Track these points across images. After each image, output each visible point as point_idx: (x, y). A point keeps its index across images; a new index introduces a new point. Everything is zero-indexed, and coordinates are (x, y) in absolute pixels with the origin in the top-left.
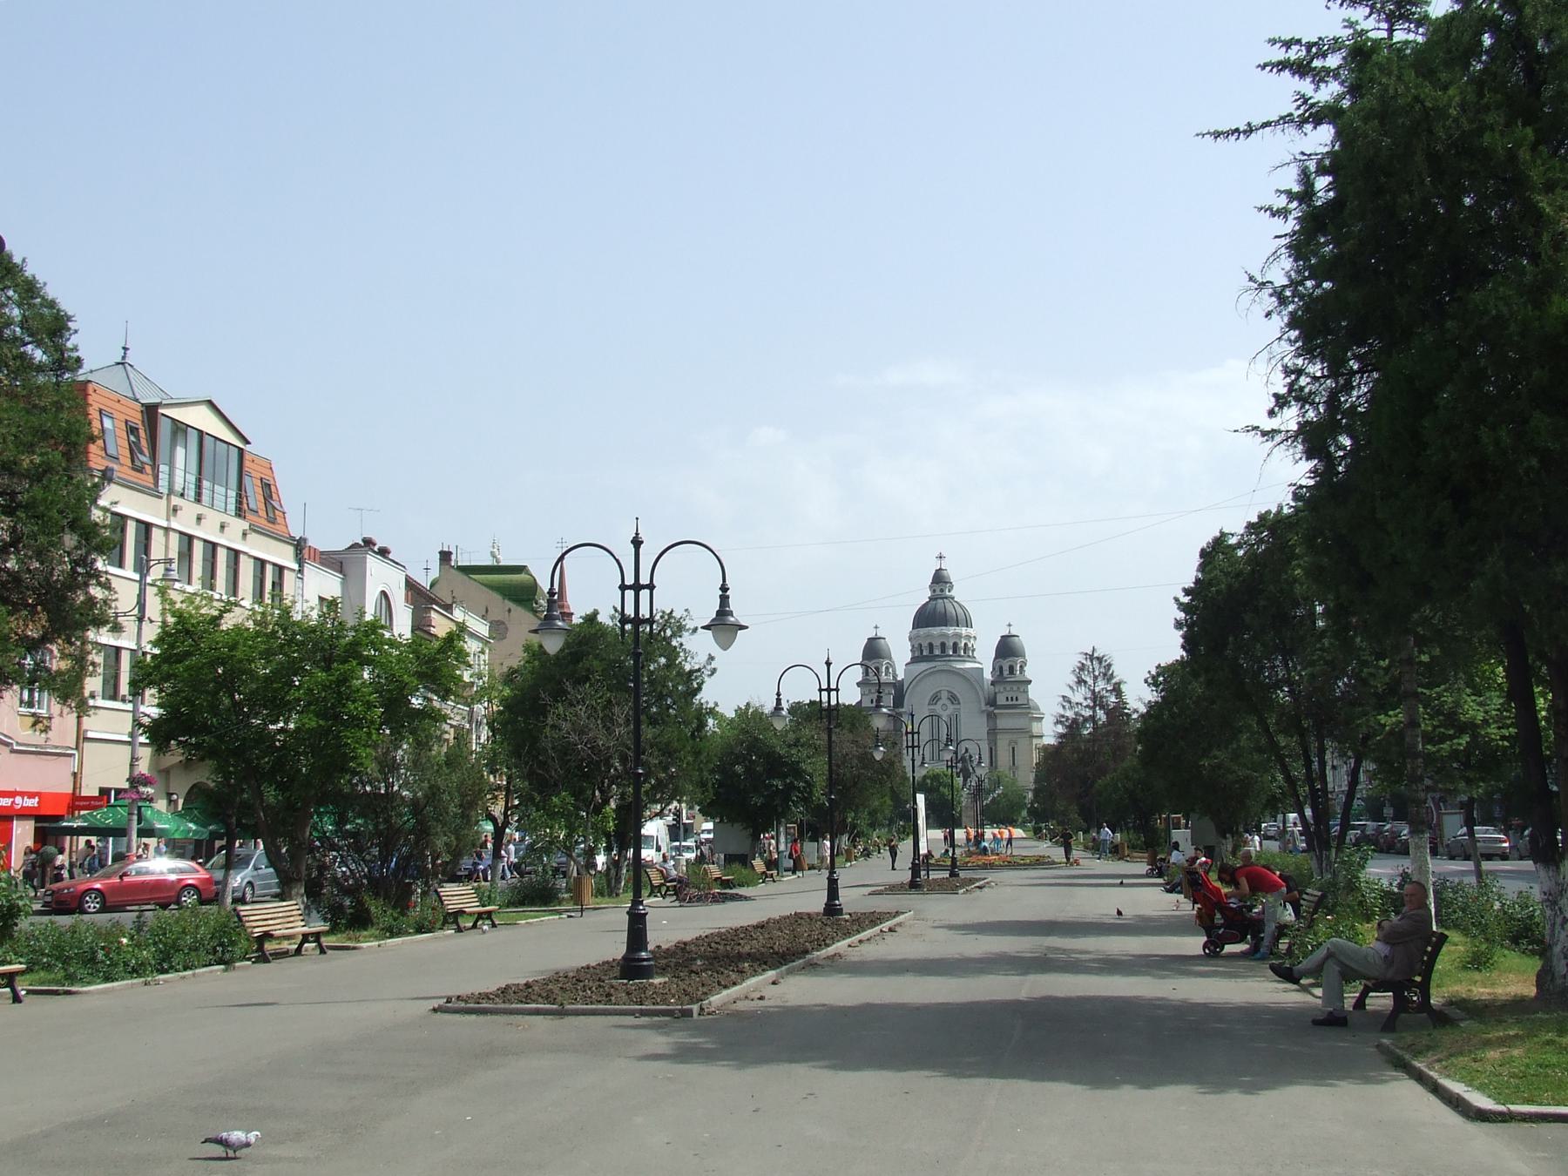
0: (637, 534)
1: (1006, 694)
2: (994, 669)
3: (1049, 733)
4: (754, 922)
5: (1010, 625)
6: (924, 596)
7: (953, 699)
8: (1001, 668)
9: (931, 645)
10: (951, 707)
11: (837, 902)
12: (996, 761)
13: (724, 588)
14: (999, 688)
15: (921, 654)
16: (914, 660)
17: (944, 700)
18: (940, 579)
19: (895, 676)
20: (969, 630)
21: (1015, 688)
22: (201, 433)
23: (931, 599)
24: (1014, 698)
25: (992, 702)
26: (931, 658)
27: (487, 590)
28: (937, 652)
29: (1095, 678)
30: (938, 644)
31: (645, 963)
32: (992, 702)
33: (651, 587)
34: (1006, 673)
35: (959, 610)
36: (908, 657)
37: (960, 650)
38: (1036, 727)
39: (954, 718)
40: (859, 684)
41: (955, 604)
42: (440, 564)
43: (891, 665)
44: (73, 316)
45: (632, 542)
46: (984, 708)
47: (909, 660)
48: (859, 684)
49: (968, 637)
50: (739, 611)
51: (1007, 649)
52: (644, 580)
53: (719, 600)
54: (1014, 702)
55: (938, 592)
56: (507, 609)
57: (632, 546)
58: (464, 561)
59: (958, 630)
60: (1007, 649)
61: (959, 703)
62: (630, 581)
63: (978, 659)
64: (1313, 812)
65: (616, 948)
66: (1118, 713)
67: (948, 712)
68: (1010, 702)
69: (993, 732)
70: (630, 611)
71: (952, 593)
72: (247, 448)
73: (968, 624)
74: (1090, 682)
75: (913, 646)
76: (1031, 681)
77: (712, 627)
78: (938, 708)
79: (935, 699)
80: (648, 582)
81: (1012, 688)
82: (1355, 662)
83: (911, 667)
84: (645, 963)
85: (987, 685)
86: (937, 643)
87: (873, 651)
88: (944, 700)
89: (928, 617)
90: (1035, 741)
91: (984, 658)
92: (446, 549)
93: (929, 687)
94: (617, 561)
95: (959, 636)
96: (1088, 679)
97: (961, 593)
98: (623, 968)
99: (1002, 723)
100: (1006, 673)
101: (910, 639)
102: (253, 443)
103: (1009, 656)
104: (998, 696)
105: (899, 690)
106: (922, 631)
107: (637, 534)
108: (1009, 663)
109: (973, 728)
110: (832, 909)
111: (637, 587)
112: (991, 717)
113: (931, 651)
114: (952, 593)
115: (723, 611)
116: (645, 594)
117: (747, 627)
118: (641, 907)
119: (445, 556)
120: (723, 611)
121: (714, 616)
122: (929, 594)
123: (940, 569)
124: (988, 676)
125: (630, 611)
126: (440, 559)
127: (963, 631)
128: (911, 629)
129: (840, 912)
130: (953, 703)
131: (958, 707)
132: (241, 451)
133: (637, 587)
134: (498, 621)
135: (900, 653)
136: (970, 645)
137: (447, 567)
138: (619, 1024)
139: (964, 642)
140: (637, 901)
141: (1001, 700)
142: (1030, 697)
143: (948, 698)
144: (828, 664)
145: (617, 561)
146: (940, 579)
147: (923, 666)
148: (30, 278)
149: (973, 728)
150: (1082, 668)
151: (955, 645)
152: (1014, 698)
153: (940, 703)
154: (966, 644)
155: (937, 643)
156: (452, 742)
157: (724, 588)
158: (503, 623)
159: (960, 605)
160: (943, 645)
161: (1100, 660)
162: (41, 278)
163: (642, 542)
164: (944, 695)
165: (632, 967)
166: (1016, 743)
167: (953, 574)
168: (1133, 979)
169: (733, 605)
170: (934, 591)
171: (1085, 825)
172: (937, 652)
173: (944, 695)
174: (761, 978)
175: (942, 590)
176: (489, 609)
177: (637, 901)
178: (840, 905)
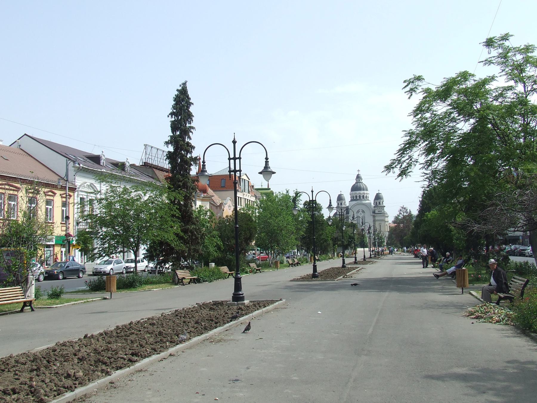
0: (234, 139)
1: (378, 210)
2: (374, 202)
3: (390, 219)
4: (337, 266)
6: (354, 182)
7: (363, 212)
8: (376, 203)
9: (356, 196)
10: (363, 214)
13: (267, 159)
15: (354, 199)
16: (351, 200)
18: (358, 177)
20: (367, 192)
22: (244, 180)
23: (356, 183)
25: (374, 212)
26: (356, 200)
28: (358, 198)
29: (404, 212)
31: (241, 296)
32: (374, 212)
33: (240, 158)
34: (378, 204)
36: (350, 199)
37: (364, 197)
38: (386, 219)
39: (363, 218)
45: (232, 142)
46: (372, 214)
47: (350, 200)
49: (367, 194)
50: (272, 166)
51: (378, 197)
52: (237, 156)
53: (265, 163)
54: (380, 212)
55: (358, 181)
57: (233, 143)
58: (255, 187)
59: (364, 192)
60: (378, 197)
62: (232, 156)
63: (370, 200)
64: (228, 268)
65: (311, 272)
66: (410, 215)
68: (379, 212)
69: (374, 221)
70: (232, 168)
71: (362, 181)
72: (249, 181)
73: (367, 190)
74: (403, 214)
77: (262, 173)
78: (359, 214)
79: (358, 212)
80: (239, 157)
81: (380, 209)
83: (351, 202)
84: (241, 296)
85: (372, 207)
86: (358, 196)
87: (340, 198)
89: (355, 188)
90: (386, 223)
91: (371, 199)
93: (355, 210)
94: (227, 149)
95: (364, 193)
96: (402, 213)
97: (365, 181)
98: (312, 276)
99: (377, 218)
100: (378, 204)
104: (376, 211)
105: (347, 209)
106: (354, 192)
107: (234, 139)
109: (369, 221)
110: (237, 297)
111: (235, 159)
112: (374, 216)
113: (356, 198)
114: (362, 181)
115: (267, 167)
116: (237, 161)
117: (275, 173)
118: (239, 275)
120: (267, 167)
121: (263, 169)
123: (359, 174)
124: (372, 205)
125: (232, 168)
127: (365, 192)
129: (242, 299)
132: (248, 181)
133: (235, 159)
139: (366, 195)
140: (315, 263)
141: (376, 212)
142: (385, 210)
144: (312, 192)
145: (227, 149)
146: (358, 177)
147: (354, 202)
149: (369, 221)
150: (401, 210)
151: (363, 196)
154: (366, 196)
155: (358, 196)
157: (267, 159)
159: (364, 184)
160: (360, 196)
161: (405, 208)
163: (236, 142)
164: (361, 211)
165: (314, 276)
166: (381, 224)
167: (362, 176)
169: (270, 164)
171: (401, 247)
172: (358, 198)
173: (361, 211)
174: (248, 316)
175: (359, 180)
177: (315, 263)
178: (243, 294)
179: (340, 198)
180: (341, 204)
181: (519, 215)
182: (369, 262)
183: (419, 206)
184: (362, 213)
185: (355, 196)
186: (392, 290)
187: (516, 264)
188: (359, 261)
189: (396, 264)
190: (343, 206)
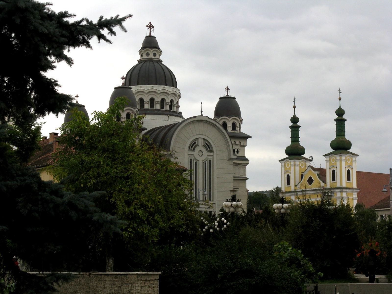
7: (208, 146)
10: (206, 153)
11: (353, 227)
12: (213, 197)
17: (201, 147)
21: (237, 142)
24: (236, 150)
28: (147, 106)
30: (148, 99)
41: (162, 65)
44: (118, 16)
48: (291, 137)
61: (212, 151)
67: (204, 157)
76: (300, 127)
78: (196, 153)
79: (193, 146)
82: (313, 238)
88: (201, 147)
102: (113, 43)
103: (235, 115)
108: (129, 111)
122: (138, 57)
123: (150, 36)
127: (170, 89)
130: (207, 150)
131: (211, 154)
136: (175, 102)
143: (194, 149)
152: (236, 150)
153: (197, 149)
154: (172, 101)
155: (147, 99)
156: (106, 145)
170: (142, 55)
184: (204, 150)
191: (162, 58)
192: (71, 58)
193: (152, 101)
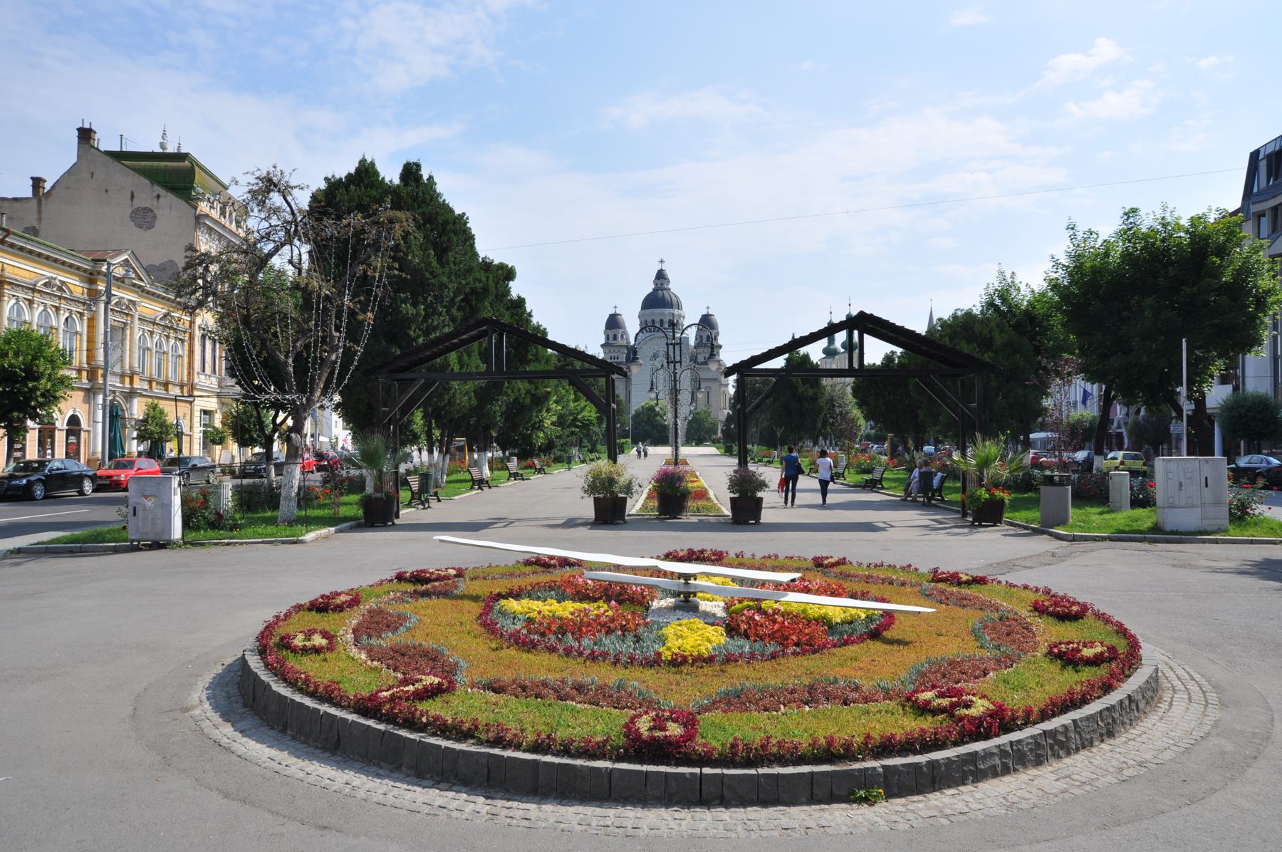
5: (708, 308)
6: (650, 288)
8: (701, 337)
14: (700, 350)
15: (647, 327)
18: (661, 276)
19: (628, 342)
20: (680, 311)
27: (132, 172)
35: (674, 298)
40: (602, 346)
42: (79, 143)
43: (625, 333)
48: (602, 346)
49: (680, 316)
51: (707, 322)
56: (156, 194)
59: (672, 311)
60: (707, 322)
73: (679, 307)
75: (641, 322)
86: (657, 320)
87: (613, 323)
92: (87, 126)
97: (676, 287)
101: (639, 317)
113: (662, 325)
114: (670, 286)
119: (85, 135)
126: (79, 137)
127: (676, 312)
128: (640, 310)
134: (146, 208)
135: (632, 326)
137: (86, 146)
138: (895, 647)
146: (661, 276)
148: (536, 325)
155: (657, 320)
158: (151, 210)
162: (544, 325)
167: (670, 274)
168: (824, 766)
172: (658, 325)
175: (662, 284)
176: (135, 195)
179: (613, 323)
180: (615, 337)
181: (198, 321)
182: (936, 506)
183: (874, 364)
185: (649, 320)
186: (1192, 530)
187: (1055, 286)
188: (829, 504)
189: (1005, 535)
190: (620, 341)
191: (670, 286)
192: (1062, 250)
193: (662, 321)
